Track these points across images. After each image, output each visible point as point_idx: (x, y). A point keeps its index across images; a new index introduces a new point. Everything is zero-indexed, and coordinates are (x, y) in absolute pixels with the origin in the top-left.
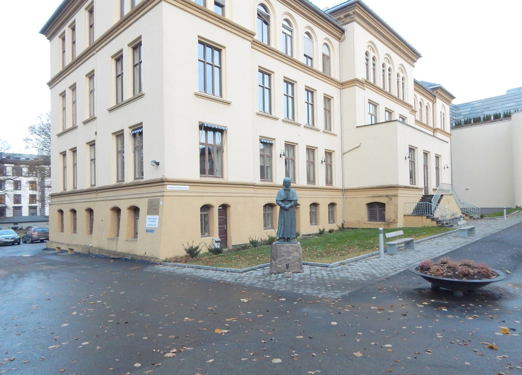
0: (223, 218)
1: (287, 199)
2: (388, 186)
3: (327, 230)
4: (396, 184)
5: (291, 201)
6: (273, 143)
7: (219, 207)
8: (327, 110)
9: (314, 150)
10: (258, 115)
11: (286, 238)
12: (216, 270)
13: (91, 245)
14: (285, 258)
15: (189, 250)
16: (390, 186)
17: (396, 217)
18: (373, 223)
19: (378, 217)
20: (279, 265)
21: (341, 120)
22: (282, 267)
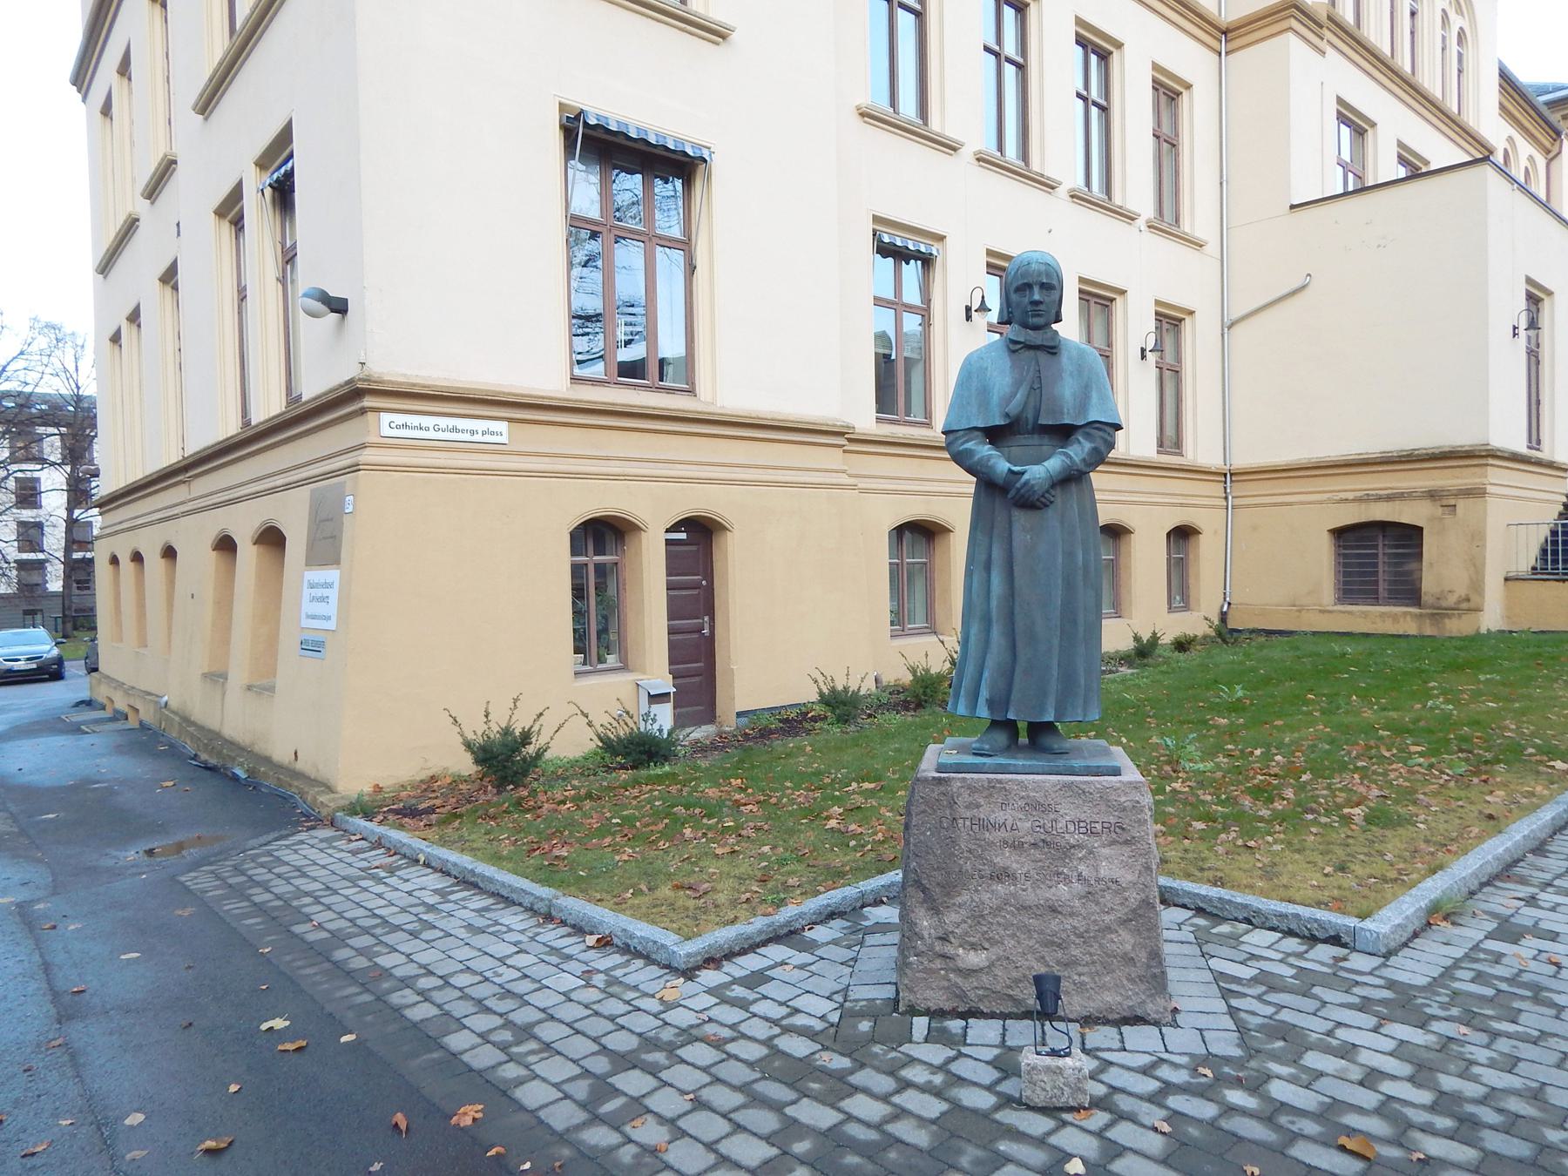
0: (697, 586)
1: (1037, 417)
2: (1437, 451)
3: (1166, 639)
4: (1476, 442)
5: (1064, 433)
6: (935, 253)
7: (667, 531)
8: (1165, 141)
9: (1112, 300)
10: (866, 119)
11: (1022, 726)
12: (549, 918)
13: (166, 698)
14: (1014, 895)
15: (483, 749)
16: (1447, 449)
17: (1477, 585)
18: (1363, 612)
19: (1382, 587)
20: (973, 947)
21: (1221, 183)
22: (992, 965)
